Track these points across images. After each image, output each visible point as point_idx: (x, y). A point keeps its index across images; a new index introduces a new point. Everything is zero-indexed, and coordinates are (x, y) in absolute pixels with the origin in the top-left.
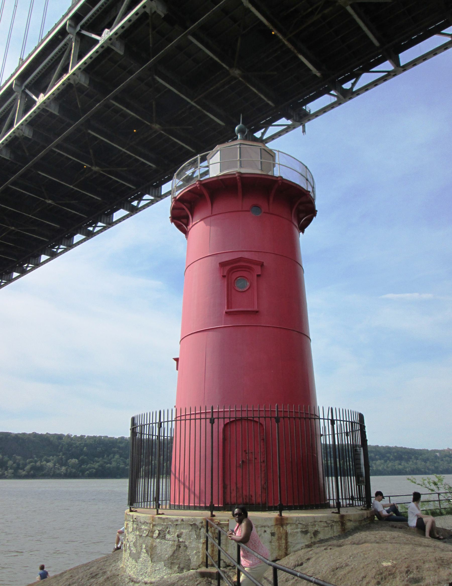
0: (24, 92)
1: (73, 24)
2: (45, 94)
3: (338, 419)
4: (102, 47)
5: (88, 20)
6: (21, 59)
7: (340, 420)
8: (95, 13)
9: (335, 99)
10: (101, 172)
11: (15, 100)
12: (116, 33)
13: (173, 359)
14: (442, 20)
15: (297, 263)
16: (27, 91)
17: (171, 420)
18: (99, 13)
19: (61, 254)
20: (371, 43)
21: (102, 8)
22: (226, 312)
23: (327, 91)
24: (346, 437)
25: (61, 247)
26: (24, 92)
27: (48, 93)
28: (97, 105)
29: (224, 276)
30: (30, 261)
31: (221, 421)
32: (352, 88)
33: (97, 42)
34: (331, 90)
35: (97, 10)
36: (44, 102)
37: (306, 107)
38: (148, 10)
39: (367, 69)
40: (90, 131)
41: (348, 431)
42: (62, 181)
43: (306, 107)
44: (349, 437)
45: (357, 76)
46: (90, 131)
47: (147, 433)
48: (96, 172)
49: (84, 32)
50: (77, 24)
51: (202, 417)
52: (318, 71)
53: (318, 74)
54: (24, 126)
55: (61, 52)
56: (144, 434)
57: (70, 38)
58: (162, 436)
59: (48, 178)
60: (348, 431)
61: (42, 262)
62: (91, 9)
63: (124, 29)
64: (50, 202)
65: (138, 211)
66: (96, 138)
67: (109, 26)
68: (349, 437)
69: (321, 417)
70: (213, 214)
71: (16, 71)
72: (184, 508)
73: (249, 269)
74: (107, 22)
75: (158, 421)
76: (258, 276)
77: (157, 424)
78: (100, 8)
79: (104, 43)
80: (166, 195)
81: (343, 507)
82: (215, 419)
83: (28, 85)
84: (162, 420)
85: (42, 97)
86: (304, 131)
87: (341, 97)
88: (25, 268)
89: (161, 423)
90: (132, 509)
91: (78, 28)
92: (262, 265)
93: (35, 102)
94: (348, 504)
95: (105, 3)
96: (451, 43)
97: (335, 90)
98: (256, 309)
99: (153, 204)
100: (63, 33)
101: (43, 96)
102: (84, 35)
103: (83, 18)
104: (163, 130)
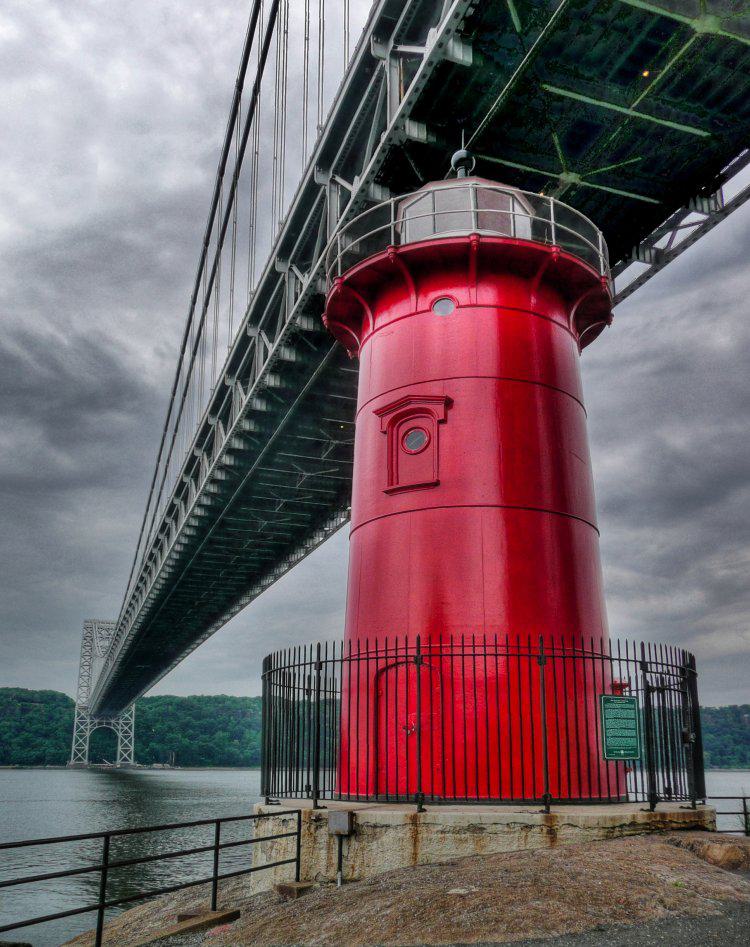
3: (653, 660)
4: (430, 63)
5: (404, 24)
6: (319, 128)
7: (657, 663)
12: (447, 31)
15: (505, 507)
17: (370, 661)
31: (372, 663)
49: (402, 48)
51: (499, 652)
63: (427, 78)
69: (615, 655)
71: (295, 200)
75: (315, 659)
77: (313, 665)
84: (323, 659)
89: (321, 664)
91: (391, 44)
95: (413, 6)
100: (368, 63)
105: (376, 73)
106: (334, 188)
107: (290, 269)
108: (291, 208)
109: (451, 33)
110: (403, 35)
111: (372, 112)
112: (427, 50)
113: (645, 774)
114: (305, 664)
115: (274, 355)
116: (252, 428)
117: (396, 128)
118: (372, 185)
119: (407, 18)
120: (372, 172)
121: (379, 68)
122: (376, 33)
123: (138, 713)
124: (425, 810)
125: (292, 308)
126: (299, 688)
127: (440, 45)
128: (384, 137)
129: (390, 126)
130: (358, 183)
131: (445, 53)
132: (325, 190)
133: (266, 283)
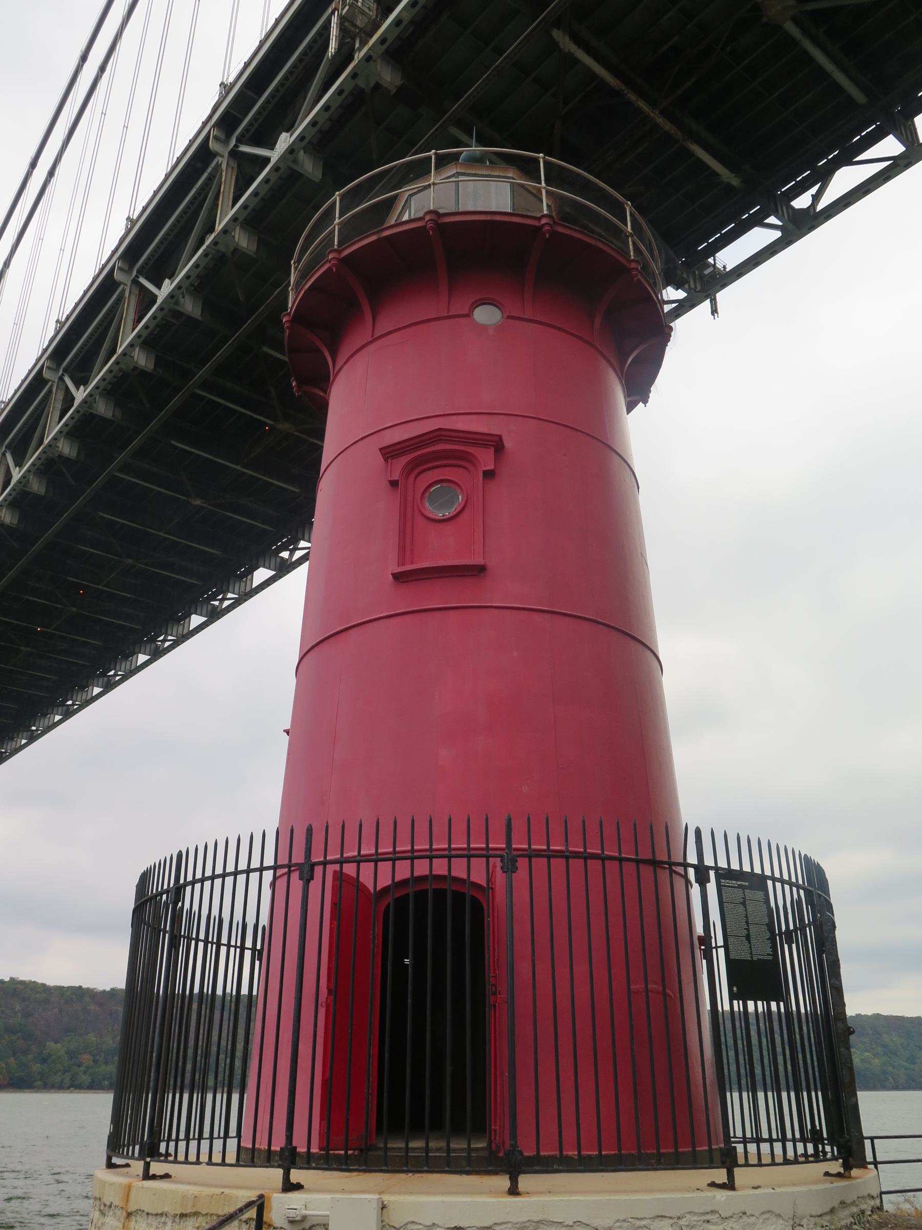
0: (135, 282)
1: (223, 136)
2: (173, 279)
4: (276, 168)
8: (263, 107)
9: (777, 234)
11: (120, 299)
12: (301, 138)
13: (284, 731)
14: (712, 241)
16: (143, 281)
19: (229, 612)
22: (397, 577)
23: (758, 221)
24: (786, 946)
25: (230, 595)
26: (135, 282)
27: (91, 384)
28: (275, 293)
29: (394, 484)
33: (267, 160)
34: (768, 216)
35: (267, 101)
36: (171, 296)
37: (714, 260)
38: (361, 83)
39: (847, 159)
41: (792, 927)
42: (217, 458)
43: (714, 260)
44: (794, 946)
45: (824, 177)
47: (239, 944)
50: (229, 136)
52: (733, 175)
53: (735, 182)
54: (183, 290)
55: (202, 196)
56: (197, 940)
57: (218, 162)
58: (212, 943)
59: (191, 453)
60: (792, 927)
62: (257, 101)
63: (318, 127)
64: (198, 502)
67: (171, 276)
68: (794, 946)
70: (376, 335)
72: (269, 1160)
73: (463, 459)
76: (489, 475)
78: (272, 96)
79: (162, 303)
81: (747, 1165)
82: (316, 868)
83: (142, 267)
84: (317, 858)
85: (167, 287)
86: (714, 311)
87: (791, 227)
88: (160, 643)
90: (115, 1160)
91: (233, 142)
92: (497, 445)
93: (154, 298)
94: (802, 1155)
98: (479, 561)
101: (168, 283)
103: (241, 121)
105: (209, 170)
106: (61, 383)
107: (61, 379)
108: (16, 391)
109: (239, 222)
112: (275, 155)
113: (820, 1094)
114: (248, 871)
115: (19, 482)
117: (225, 231)
118: (137, 349)
119: (255, 118)
120: (187, 276)
121: (213, 164)
122: (123, 257)
124: (298, 1187)
125: (53, 429)
126: (229, 946)
127: (291, 150)
128: (210, 239)
129: (219, 227)
130: (168, 286)
132: (124, 290)
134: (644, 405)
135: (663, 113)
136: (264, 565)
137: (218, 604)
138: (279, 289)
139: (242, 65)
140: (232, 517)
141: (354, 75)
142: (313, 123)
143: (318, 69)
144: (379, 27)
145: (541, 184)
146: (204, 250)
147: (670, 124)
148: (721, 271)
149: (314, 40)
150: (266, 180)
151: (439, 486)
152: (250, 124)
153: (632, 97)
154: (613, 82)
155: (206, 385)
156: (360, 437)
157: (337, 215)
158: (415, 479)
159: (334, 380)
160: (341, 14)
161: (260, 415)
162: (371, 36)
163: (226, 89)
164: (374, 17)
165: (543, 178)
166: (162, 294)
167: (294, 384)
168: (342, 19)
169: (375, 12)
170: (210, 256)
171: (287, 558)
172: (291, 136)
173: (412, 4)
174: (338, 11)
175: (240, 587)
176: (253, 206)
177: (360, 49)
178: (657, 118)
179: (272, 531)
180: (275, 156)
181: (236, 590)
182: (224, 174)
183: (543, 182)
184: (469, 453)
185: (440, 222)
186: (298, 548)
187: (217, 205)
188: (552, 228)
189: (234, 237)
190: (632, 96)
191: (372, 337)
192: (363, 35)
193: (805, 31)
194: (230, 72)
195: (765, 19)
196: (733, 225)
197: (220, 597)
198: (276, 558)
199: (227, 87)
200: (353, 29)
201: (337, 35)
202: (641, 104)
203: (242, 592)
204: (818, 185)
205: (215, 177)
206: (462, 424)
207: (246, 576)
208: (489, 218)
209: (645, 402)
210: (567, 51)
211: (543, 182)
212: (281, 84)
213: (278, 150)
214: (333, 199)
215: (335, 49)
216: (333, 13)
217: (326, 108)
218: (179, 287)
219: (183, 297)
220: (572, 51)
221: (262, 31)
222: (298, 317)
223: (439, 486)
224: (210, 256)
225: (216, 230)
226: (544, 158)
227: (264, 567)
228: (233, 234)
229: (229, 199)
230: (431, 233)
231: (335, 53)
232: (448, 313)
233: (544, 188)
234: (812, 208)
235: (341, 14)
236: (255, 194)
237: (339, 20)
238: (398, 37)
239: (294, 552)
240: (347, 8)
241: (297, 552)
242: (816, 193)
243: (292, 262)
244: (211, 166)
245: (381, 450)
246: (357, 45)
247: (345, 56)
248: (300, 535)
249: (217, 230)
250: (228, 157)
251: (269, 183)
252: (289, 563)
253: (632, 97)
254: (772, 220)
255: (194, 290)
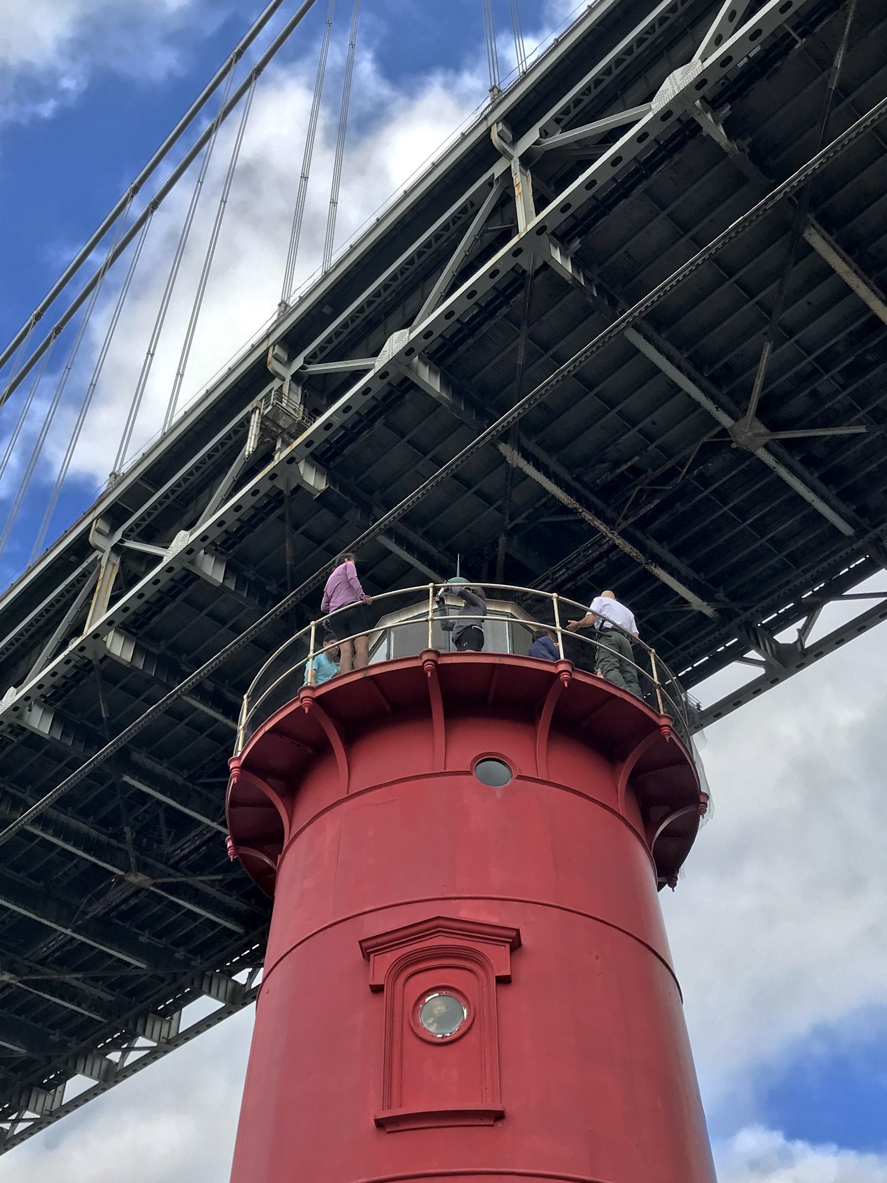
1: (106, 529)
2: (19, 688)
4: (169, 569)
6: (283, 304)
8: (159, 502)
9: (761, 671)
10: (152, 888)
12: (203, 538)
18: (168, 502)
20: (835, 531)
21: (152, 513)
23: (737, 654)
28: (148, 711)
30: (32, 1100)
32: (801, 640)
33: (159, 559)
34: (748, 650)
35: (166, 496)
38: (280, 484)
40: (127, 778)
45: (811, 609)
46: (127, 778)
48: (139, 891)
55: (61, 603)
57: (96, 557)
61: (127, 1067)
62: (153, 494)
63: (144, 599)
65: (120, 1078)
66: (144, 797)
67: (408, 323)
74: (187, 518)
76: (504, 981)
78: (172, 490)
80: (145, 1062)
87: (776, 663)
91: (118, 535)
95: (672, 8)
96: (882, 617)
97: (757, 647)
99: (156, 1059)
102: (130, 550)
104: (20, 982)
109: (115, 625)
110: (137, 531)
111: (68, 605)
112: (169, 555)
116: (128, 656)
117: (96, 635)
120: (40, 686)
123: (93, 1009)
127: (189, 550)
129: (88, 630)
131: (192, 562)
133: (591, 31)
134: (671, 889)
135: (623, 534)
136: (83, 1072)
137: (8, 1129)
138: (154, 706)
139: (139, 456)
140: (49, 1000)
141: (272, 476)
142: (220, 523)
143: (231, 465)
144: (305, 429)
145: (556, 626)
146: (66, 656)
147: (630, 546)
148: (695, 709)
149: (228, 437)
150: (155, 581)
151: (437, 995)
152: (142, 518)
153: (588, 516)
154: (566, 499)
155: (41, 820)
156: (329, 923)
157: (312, 648)
158: (404, 986)
159: (291, 843)
160: (263, 413)
161: (107, 863)
162: (296, 438)
163: (117, 480)
164: (300, 418)
165: (557, 620)
166: (3, 704)
167: (229, 844)
168: (264, 418)
169: (301, 414)
170: (71, 664)
171: (117, 1061)
172: (191, 535)
173: (783, 8)
174: (260, 410)
175: (45, 1101)
176: (134, 610)
177: (281, 450)
178: (616, 539)
179: (101, 1022)
180: (170, 554)
181: (39, 1108)
182: (102, 570)
183: (558, 624)
184: (477, 952)
185: (439, 663)
186: (133, 1047)
187: (90, 604)
188: (571, 676)
189: (105, 642)
190: (587, 516)
191: (347, 794)
192: (285, 436)
193: (780, 460)
194: (124, 463)
195: (734, 445)
196: (707, 658)
197: (13, 1117)
198: (102, 1061)
199: (118, 478)
200: (274, 429)
201: (257, 434)
202: (597, 523)
203: (163, 1037)
204: (16, 1114)
205: (90, 573)
206: (466, 912)
207: (55, 1087)
208: (497, 661)
209: (673, 885)
210: (515, 466)
211: (558, 624)
212: (184, 479)
213: (173, 549)
214: (308, 628)
215: (253, 448)
216: (253, 411)
217: (237, 508)
218: (26, 698)
219: (30, 710)
220: (521, 466)
221: (165, 426)
222: (247, 765)
223: (437, 995)
224: (71, 664)
225: (84, 633)
226: (557, 598)
227: (83, 1073)
228: (104, 639)
229: (105, 599)
230: (429, 675)
231: (253, 452)
232: (445, 769)
233: (559, 630)
234: (799, 644)
235: (263, 413)
236: (140, 595)
237: (260, 419)
238: (327, 441)
239: (127, 1053)
240: (270, 407)
241: (132, 1053)
242: (802, 628)
243: (245, 696)
244: (87, 560)
245: (360, 942)
246: (278, 446)
247: (264, 456)
248: (139, 1029)
249: (86, 633)
250: (110, 553)
251: (157, 585)
252: (118, 1069)
253: (588, 516)
254: (752, 654)
255: (44, 701)
